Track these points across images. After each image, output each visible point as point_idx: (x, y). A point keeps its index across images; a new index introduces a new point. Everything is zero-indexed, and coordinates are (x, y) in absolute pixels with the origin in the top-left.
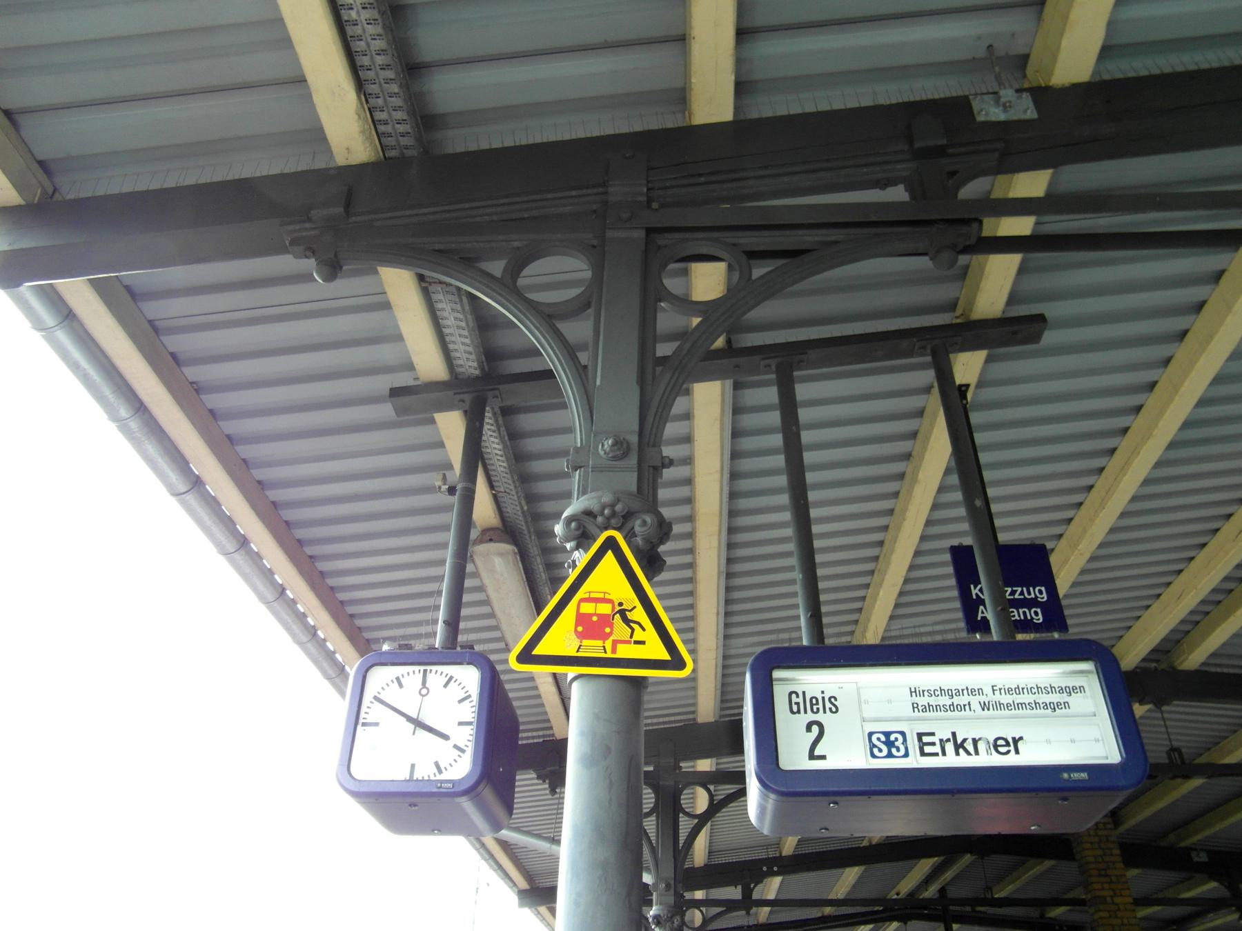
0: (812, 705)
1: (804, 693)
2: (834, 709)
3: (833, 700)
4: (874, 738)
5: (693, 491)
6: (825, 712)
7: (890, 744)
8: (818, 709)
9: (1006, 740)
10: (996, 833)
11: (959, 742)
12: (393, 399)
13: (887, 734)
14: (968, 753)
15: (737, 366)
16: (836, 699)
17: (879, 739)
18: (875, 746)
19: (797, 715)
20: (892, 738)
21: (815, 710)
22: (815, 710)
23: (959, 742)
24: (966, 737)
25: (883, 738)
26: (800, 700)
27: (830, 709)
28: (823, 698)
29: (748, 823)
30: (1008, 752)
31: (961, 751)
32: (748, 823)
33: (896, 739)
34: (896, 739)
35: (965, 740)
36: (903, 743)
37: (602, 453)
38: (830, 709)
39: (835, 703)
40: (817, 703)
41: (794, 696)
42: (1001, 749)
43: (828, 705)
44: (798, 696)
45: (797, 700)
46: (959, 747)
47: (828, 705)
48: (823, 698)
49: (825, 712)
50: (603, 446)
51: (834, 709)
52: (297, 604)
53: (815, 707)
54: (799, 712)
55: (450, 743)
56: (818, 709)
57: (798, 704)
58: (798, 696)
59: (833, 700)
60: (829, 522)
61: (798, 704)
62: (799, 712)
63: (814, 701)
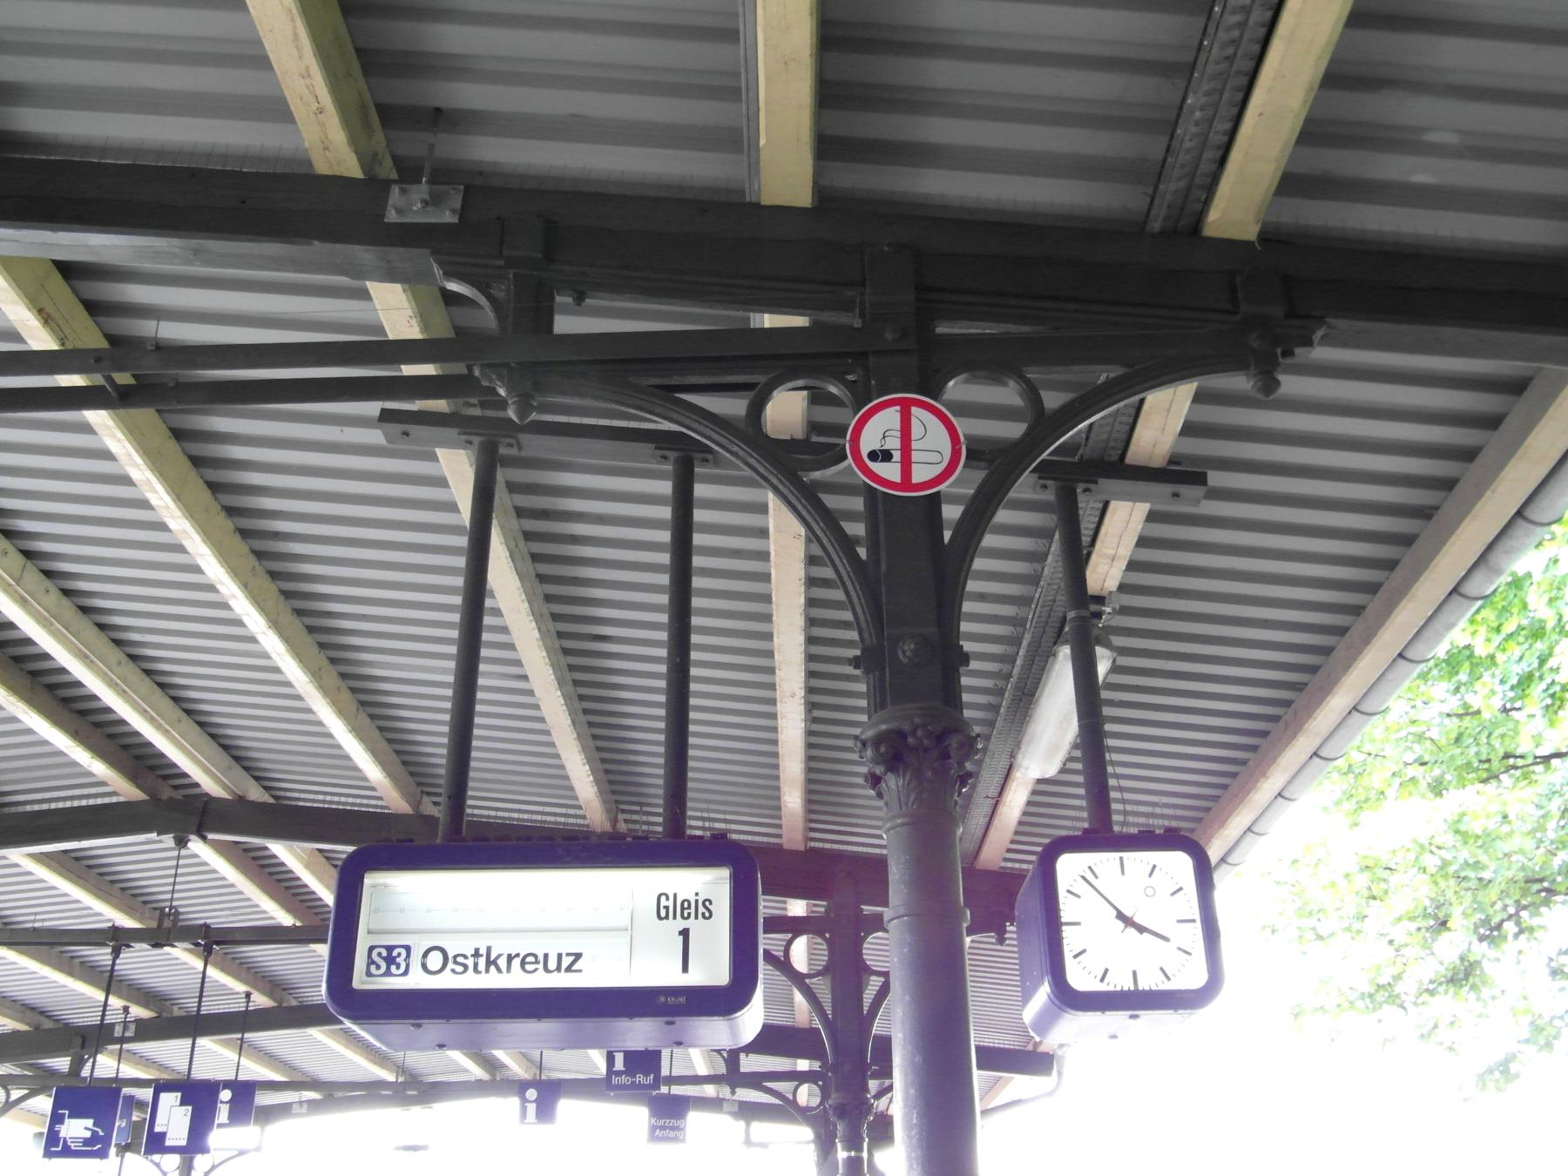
0: (683, 909)
1: (675, 895)
2: (707, 915)
3: (707, 903)
4: (375, 952)
5: (806, 681)
6: (696, 917)
7: (390, 960)
8: (689, 914)
9: (535, 956)
10: (1107, 1013)
11: (492, 959)
12: (384, 424)
13: (390, 949)
14: (499, 970)
15: (407, 434)
16: (711, 903)
17: (379, 954)
18: (373, 962)
19: (665, 920)
20: (395, 953)
21: (686, 915)
22: (686, 915)
23: (492, 959)
24: (501, 953)
25: (384, 953)
26: (670, 903)
27: (703, 914)
28: (697, 901)
29: (1020, 1021)
30: (536, 970)
31: (492, 968)
32: (1020, 1021)
33: (399, 955)
34: (399, 955)
35: (499, 956)
36: (405, 960)
37: (905, 660)
38: (703, 914)
39: (710, 907)
40: (689, 907)
41: (663, 898)
42: (528, 967)
43: (701, 910)
44: (668, 899)
45: (666, 903)
46: (490, 963)
47: (701, 910)
48: (697, 901)
49: (696, 917)
50: (904, 652)
51: (707, 915)
52: (1154, 832)
53: (686, 912)
54: (667, 917)
55: (1171, 946)
56: (689, 914)
57: (667, 908)
58: (668, 899)
59: (707, 903)
60: (168, 604)
61: (667, 908)
62: (667, 917)
63: (686, 905)
